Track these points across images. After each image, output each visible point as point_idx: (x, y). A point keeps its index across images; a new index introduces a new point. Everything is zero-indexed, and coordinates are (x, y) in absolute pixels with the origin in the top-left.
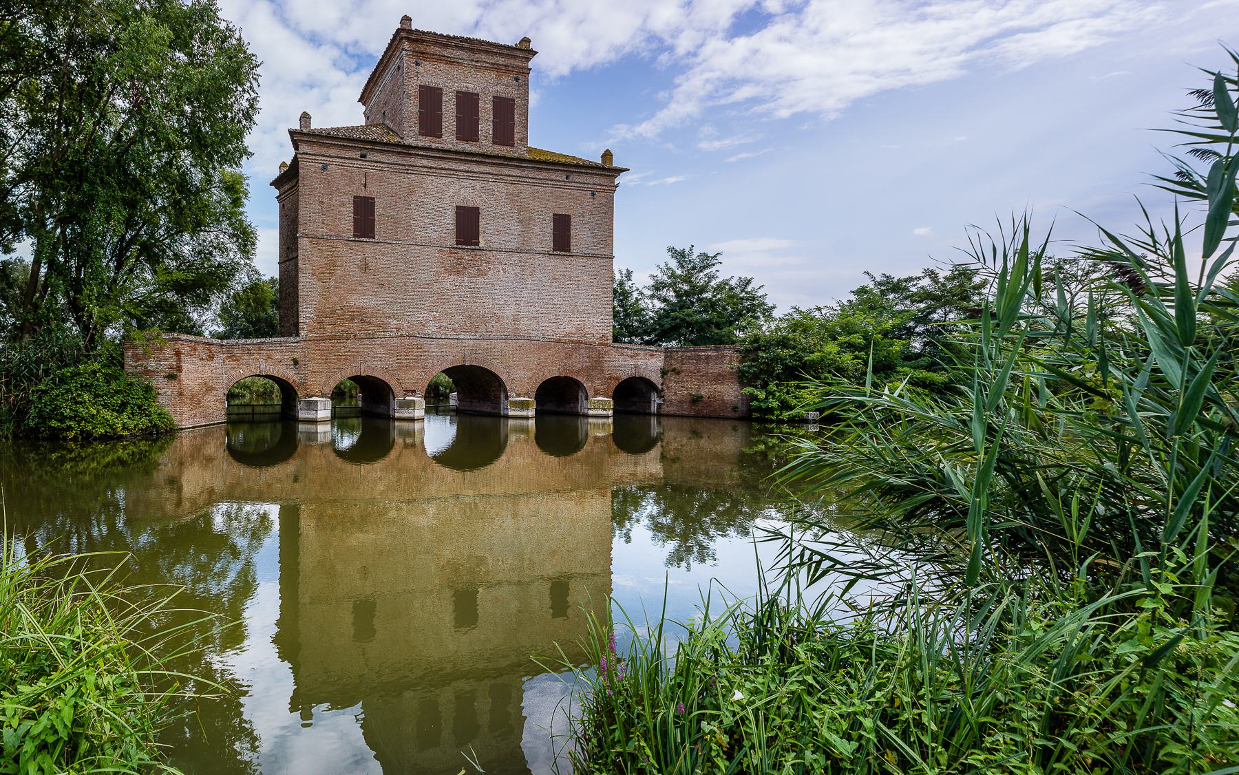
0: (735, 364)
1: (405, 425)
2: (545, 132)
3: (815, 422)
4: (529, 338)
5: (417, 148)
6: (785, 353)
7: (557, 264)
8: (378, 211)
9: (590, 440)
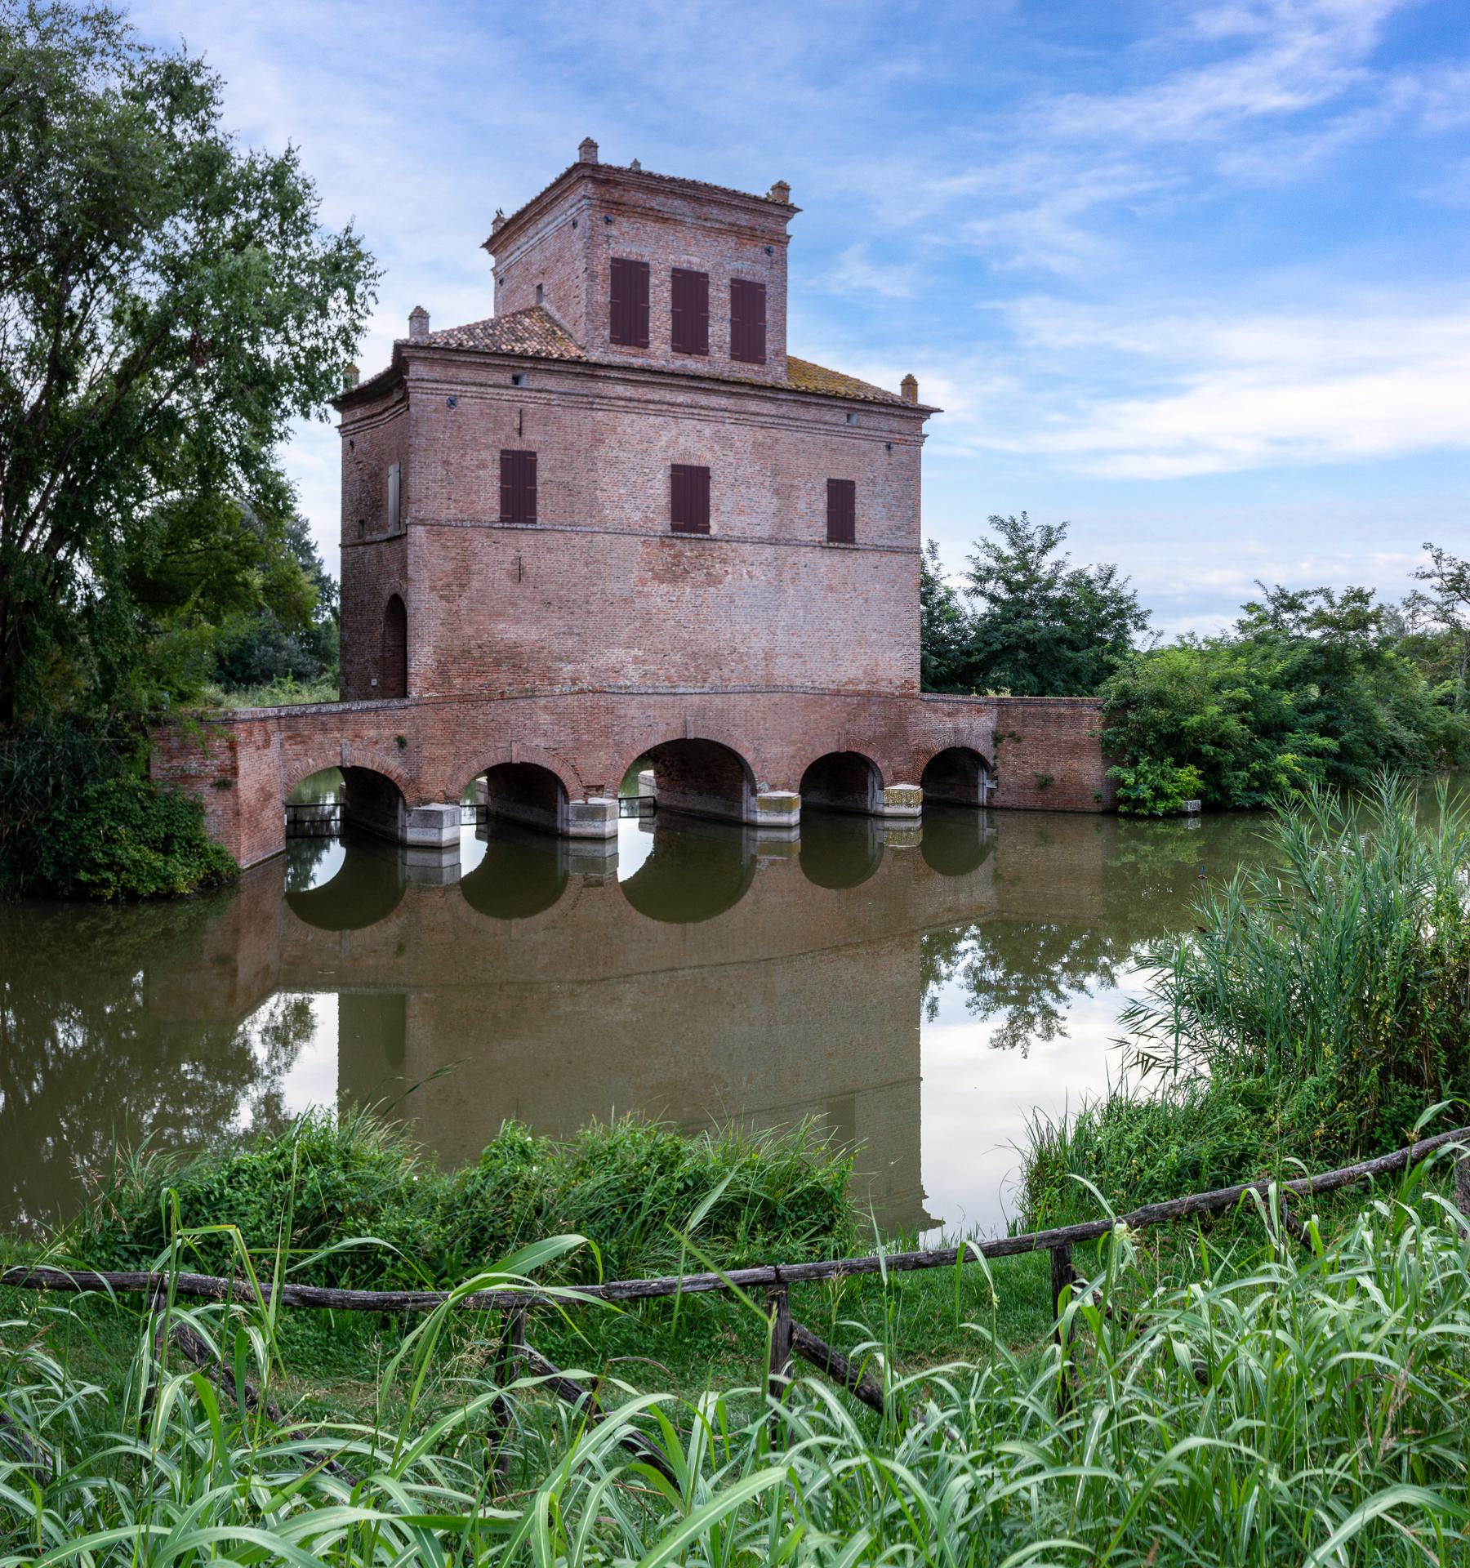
0: (1098, 728)
1: (589, 849)
2: (809, 340)
3: (1195, 814)
4: (791, 690)
5: (609, 367)
6: (1160, 714)
7: (830, 563)
8: (543, 474)
9: (888, 856)
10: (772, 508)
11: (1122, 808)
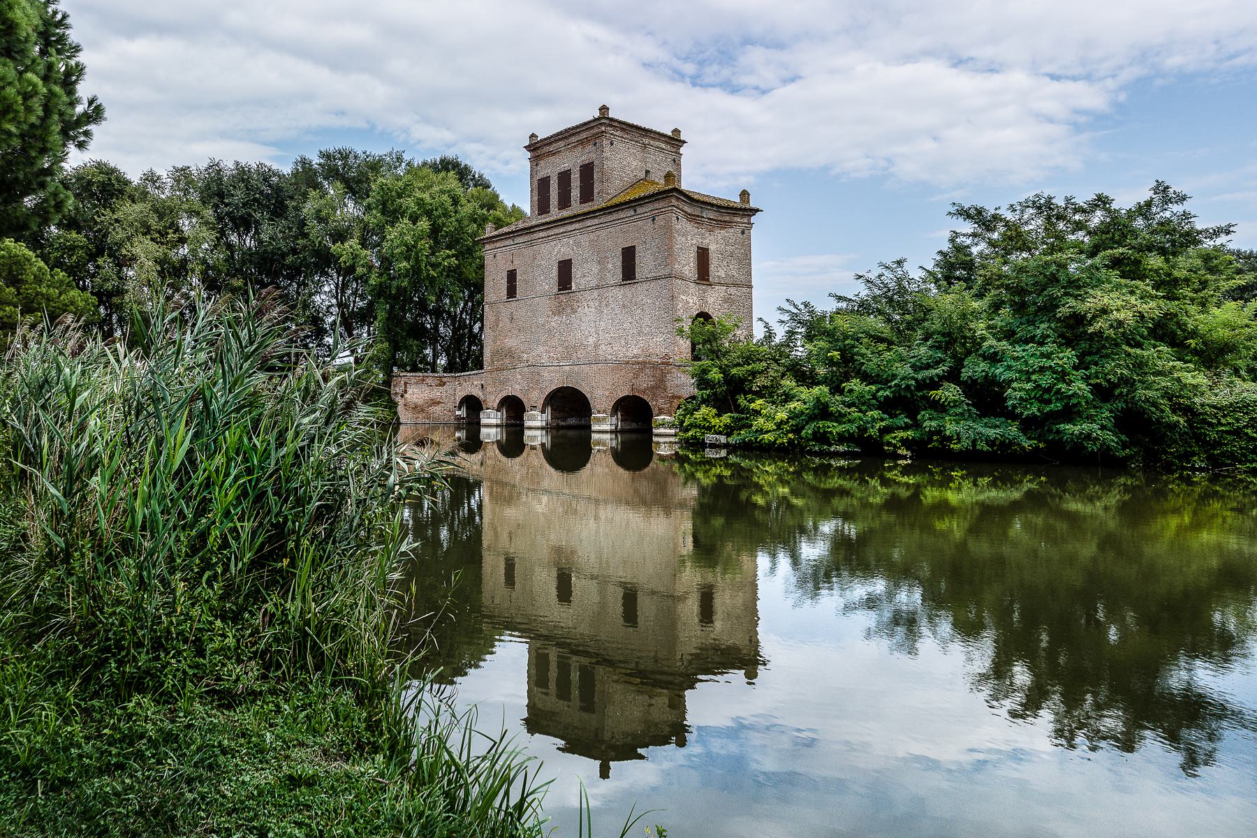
4: (606, 361)
8: (518, 278)
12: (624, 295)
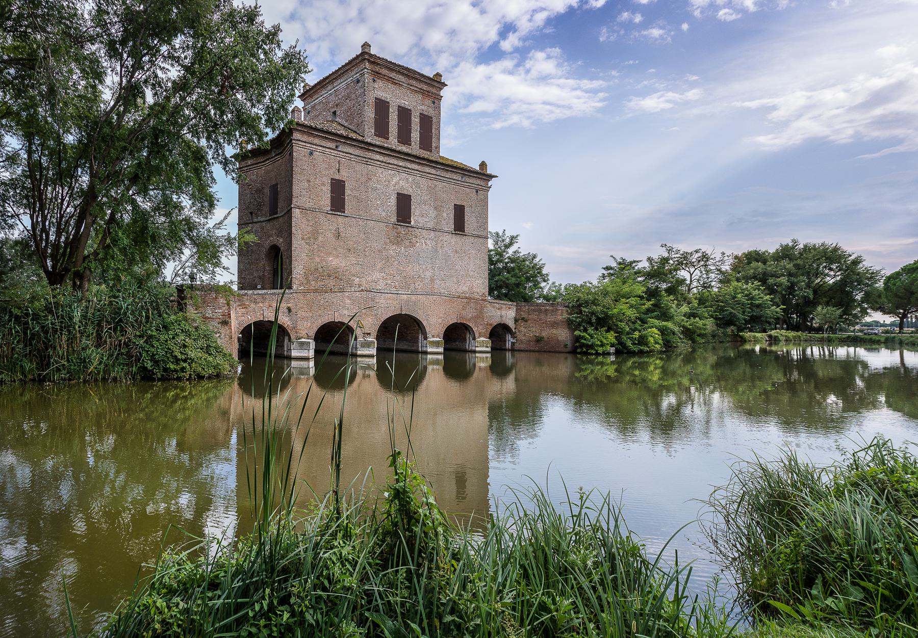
2: (450, 146)
4: (440, 295)
7: (455, 240)
8: (348, 192)
9: (477, 368)
10: (433, 215)
11: (579, 350)
12: (456, 243)
